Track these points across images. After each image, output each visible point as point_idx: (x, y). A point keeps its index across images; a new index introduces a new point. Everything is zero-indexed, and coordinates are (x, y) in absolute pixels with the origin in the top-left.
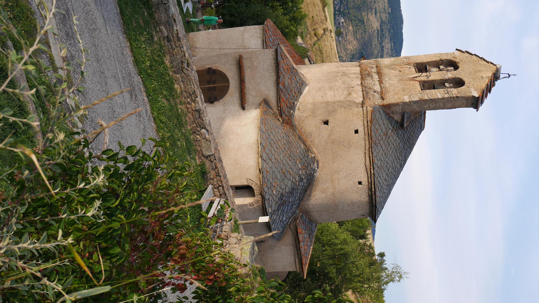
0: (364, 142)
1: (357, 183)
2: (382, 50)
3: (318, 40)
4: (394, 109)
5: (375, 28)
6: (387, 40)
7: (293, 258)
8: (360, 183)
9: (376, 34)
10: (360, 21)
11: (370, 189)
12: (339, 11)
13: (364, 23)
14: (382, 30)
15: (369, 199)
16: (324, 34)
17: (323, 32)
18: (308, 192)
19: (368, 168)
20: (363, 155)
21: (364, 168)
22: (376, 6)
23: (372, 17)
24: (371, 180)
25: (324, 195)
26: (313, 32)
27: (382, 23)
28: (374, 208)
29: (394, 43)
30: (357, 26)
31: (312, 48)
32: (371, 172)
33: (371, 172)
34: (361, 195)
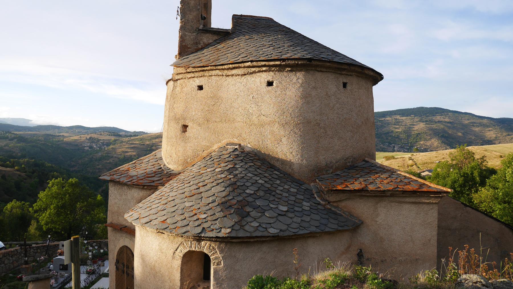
0: (213, 77)
1: (270, 88)
2: (441, 122)
3: (416, 164)
4: (189, 42)
5: (424, 126)
6: (434, 118)
7: (406, 206)
8: (270, 84)
9: (428, 126)
10: (417, 136)
11: (281, 68)
12: (408, 149)
13: (419, 133)
14: (427, 121)
15: (301, 71)
16: (413, 160)
17: (411, 161)
18: (277, 164)
19: (246, 71)
20: (230, 79)
21: (248, 77)
22: (408, 124)
23: (416, 128)
24: (265, 66)
25: (284, 140)
26: (410, 168)
27: (421, 121)
28: (313, 62)
29: (436, 113)
30: (421, 138)
31: (420, 169)
32: (249, 67)
33: (249, 67)
34: (291, 86)
